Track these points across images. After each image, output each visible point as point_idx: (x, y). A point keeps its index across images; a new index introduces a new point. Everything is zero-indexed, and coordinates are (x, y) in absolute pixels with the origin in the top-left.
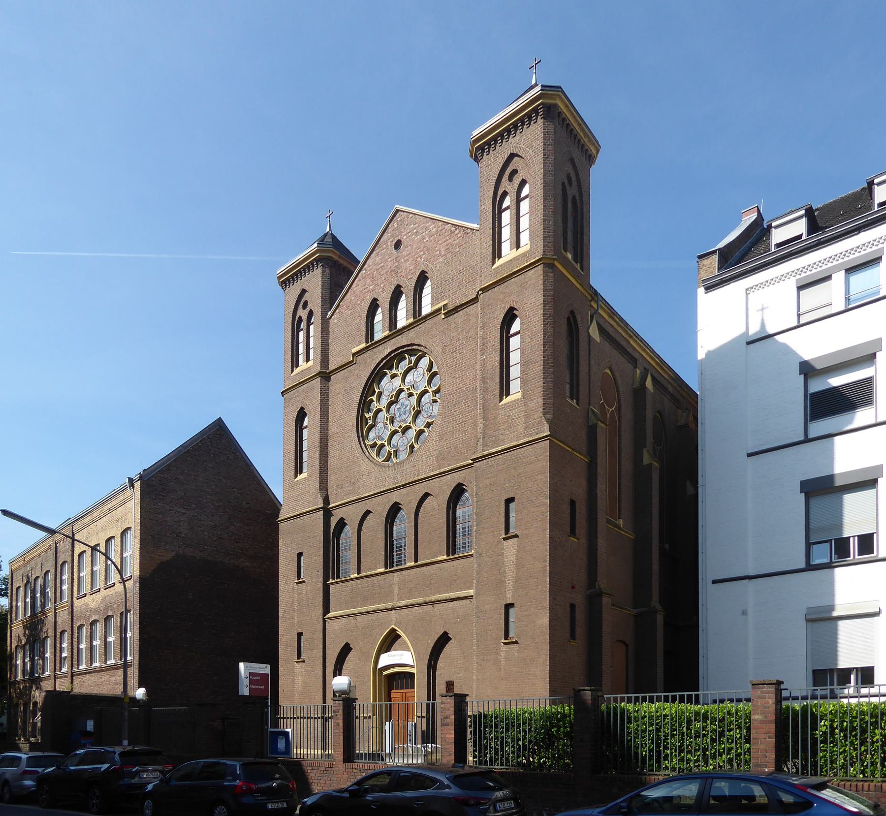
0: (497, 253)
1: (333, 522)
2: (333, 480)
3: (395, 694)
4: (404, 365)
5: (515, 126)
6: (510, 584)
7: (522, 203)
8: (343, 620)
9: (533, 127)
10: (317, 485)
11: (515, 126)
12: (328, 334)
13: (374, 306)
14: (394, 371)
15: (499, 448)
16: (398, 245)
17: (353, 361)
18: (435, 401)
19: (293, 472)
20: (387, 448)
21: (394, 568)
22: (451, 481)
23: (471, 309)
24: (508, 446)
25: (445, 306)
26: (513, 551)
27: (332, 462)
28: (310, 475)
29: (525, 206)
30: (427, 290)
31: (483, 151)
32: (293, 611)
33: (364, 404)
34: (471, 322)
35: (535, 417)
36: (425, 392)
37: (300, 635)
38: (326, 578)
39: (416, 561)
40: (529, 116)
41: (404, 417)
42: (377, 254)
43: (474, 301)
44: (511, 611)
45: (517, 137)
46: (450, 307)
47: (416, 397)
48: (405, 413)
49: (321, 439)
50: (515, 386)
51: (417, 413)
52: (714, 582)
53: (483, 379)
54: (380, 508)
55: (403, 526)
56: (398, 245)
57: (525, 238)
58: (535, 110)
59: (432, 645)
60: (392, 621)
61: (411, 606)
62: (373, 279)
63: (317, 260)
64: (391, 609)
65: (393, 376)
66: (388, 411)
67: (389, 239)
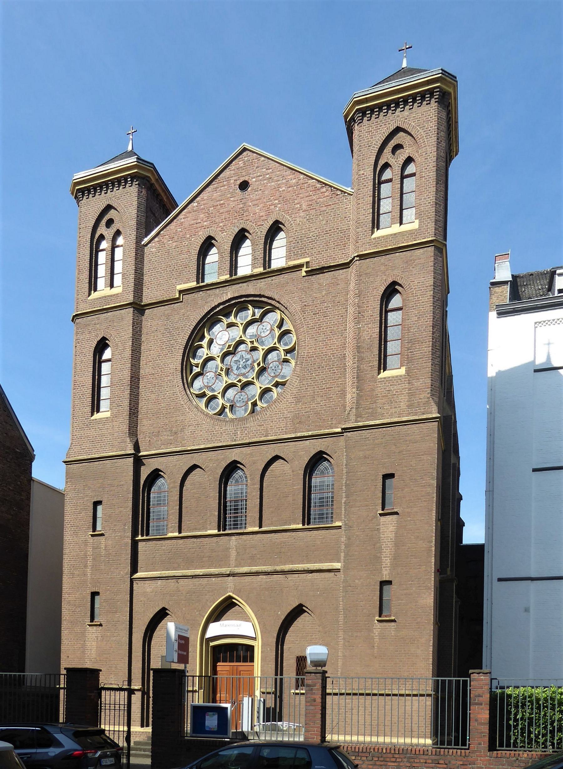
0: (93, 286)
1: (145, 473)
2: (145, 426)
3: (222, 666)
4: (250, 313)
5: (405, 101)
6: (387, 561)
7: (116, 249)
8: (160, 582)
9: (424, 107)
10: (125, 428)
11: (405, 101)
12: (142, 261)
13: (208, 244)
14: (232, 319)
15: (378, 422)
16: (244, 186)
17: (178, 299)
18: (286, 361)
19: (89, 409)
20: (220, 401)
21: (226, 532)
22: (311, 448)
23: (341, 273)
24: (388, 421)
25: (307, 263)
26: (392, 528)
27: (143, 406)
28: (114, 416)
29: (119, 253)
30: (280, 241)
31: (364, 114)
32: (86, 566)
33: (191, 349)
34: (338, 287)
35: (422, 396)
36: (273, 349)
37: (94, 594)
38: (135, 533)
39: (260, 526)
40: (423, 96)
41: (243, 371)
42: (216, 189)
43: (346, 266)
44: (97, 598)
45: (406, 113)
46: (314, 266)
47: (261, 353)
48: (245, 367)
49: (132, 377)
50: (104, 405)
51: (262, 370)
52: (500, 580)
53: (358, 348)
54: (216, 463)
55: (242, 487)
56: (244, 186)
57: (118, 280)
58: (431, 92)
59: (283, 617)
60: (230, 588)
61: (257, 573)
62: (209, 216)
63: (133, 177)
64: (229, 575)
65: (230, 325)
66: (222, 361)
67: (232, 177)
